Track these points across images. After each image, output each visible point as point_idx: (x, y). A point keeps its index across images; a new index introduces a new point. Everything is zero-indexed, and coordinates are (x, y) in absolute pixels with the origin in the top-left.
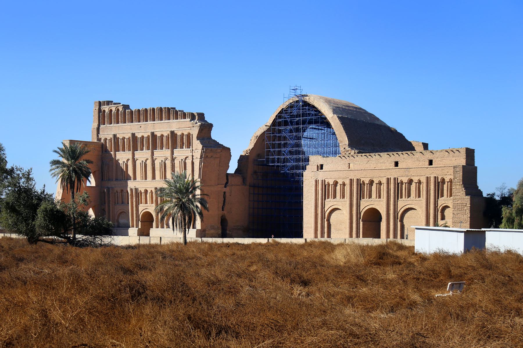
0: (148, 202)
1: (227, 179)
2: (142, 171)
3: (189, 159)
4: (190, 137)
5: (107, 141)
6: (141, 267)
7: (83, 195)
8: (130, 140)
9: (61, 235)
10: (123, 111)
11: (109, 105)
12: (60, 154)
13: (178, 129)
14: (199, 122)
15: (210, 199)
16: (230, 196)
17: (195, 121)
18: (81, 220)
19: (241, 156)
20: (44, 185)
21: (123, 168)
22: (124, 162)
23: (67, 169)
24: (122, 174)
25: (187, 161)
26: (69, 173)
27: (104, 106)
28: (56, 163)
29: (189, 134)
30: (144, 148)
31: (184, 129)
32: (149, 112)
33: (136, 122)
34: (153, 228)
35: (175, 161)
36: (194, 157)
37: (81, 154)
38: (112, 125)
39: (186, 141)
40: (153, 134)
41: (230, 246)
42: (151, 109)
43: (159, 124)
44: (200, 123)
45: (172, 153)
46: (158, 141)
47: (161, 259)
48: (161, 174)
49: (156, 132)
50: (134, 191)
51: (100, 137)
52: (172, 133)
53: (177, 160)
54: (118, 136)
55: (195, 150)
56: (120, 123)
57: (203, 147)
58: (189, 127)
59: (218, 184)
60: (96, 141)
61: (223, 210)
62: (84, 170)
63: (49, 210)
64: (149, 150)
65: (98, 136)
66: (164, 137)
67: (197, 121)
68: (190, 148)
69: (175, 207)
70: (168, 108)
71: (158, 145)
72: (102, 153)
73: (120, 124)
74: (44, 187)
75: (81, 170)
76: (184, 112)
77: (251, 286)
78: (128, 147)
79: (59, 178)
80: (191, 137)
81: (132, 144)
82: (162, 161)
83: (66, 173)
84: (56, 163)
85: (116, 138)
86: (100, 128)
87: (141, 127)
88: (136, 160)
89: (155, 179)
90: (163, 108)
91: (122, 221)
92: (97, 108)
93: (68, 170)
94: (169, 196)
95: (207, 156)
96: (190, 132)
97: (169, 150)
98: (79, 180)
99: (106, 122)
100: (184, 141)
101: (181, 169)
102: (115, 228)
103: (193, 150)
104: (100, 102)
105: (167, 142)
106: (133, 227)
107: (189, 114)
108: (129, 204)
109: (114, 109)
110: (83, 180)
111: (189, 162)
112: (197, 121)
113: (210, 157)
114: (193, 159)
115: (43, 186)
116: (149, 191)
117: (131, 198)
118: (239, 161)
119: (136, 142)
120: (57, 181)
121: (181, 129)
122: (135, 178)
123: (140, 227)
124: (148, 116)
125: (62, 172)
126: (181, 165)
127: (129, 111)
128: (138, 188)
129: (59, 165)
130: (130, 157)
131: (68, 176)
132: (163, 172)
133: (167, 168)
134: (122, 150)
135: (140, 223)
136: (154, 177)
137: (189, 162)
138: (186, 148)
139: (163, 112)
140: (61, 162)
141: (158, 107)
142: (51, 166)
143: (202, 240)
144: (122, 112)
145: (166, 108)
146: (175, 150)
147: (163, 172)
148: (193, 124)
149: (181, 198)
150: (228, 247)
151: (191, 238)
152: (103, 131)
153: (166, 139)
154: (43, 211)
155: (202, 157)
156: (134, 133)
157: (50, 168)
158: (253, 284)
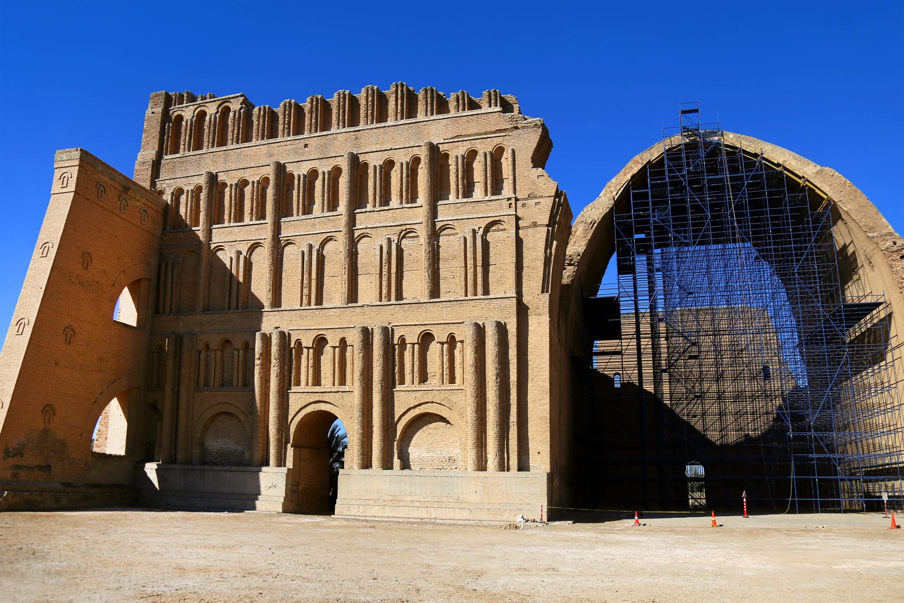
2: (306, 276)
21: (234, 272)
36: (520, 222)
55: (525, 199)
72: (163, 233)
78: (257, 207)
86: (163, 162)
88: (283, 243)
114: (518, 228)
117: (262, 365)
119: (285, 192)
128: (289, 334)
134: (235, 216)
135: (290, 451)
152: (173, 170)
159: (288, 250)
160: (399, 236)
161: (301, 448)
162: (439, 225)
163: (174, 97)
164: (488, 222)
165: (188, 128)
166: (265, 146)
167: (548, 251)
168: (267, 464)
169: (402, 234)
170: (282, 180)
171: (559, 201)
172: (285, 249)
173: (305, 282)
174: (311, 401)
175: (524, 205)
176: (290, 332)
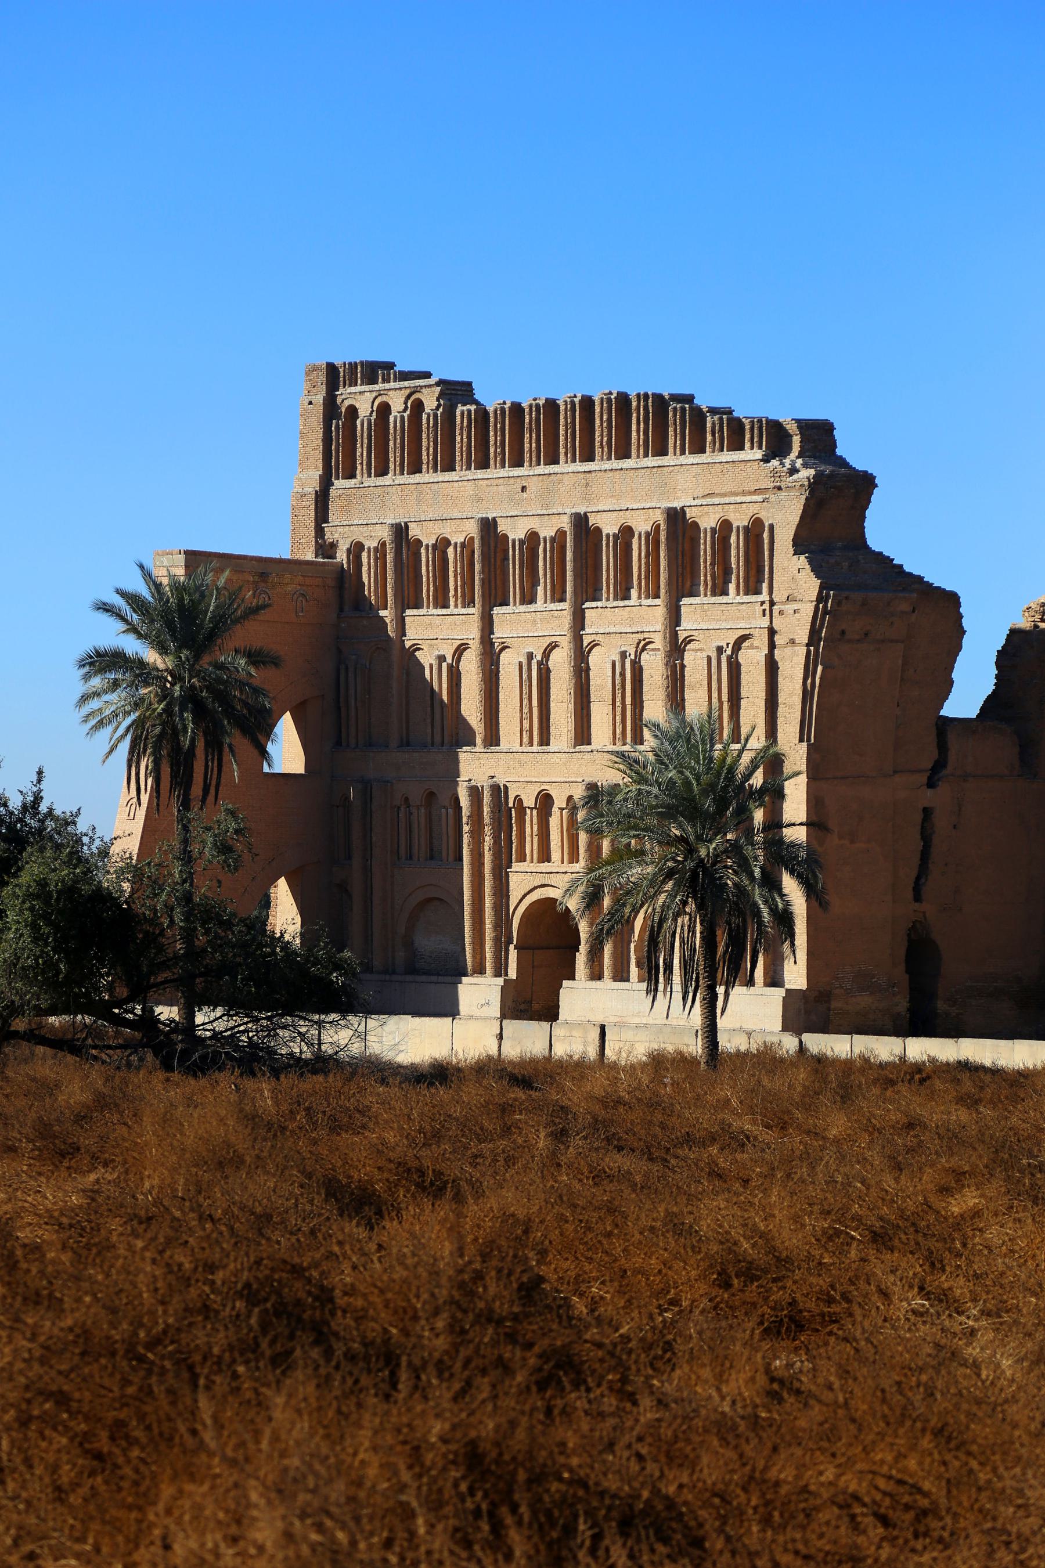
0: (555, 855)
1: (942, 746)
2: (525, 702)
3: (752, 647)
4: (759, 537)
5: (364, 555)
6: (423, 1181)
7: (218, 821)
8: (473, 552)
9: (116, 1011)
10: (441, 410)
11: (373, 381)
12: (124, 620)
13: (704, 502)
14: (805, 466)
15: (852, 842)
16: (955, 827)
17: (787, 462)
18: (208, 941)
19: (1014, 634)
20: (40, 773)
21: (436, 687)
22: (441, 659)
23: (157, 694)
24: (433, 719)
25: (743, 656)
26: (168, 711)
27: (353, 389)
28: (108, 666)
29: (757, 524)
30: (540, 590)
31: (732, 499)
32: (566, 418)
33: (503, 466)
34: (574, 979)
35: (688, 657)
36: (776, 638)
37: (223, 622)
38: (387, 480)
39: (742, 559)
40: (580, 521)
41: (929, 1077)
42: (577, 400)
43: (610, 474)
44: (812, 472)
45: (674, 617)
46: (604, 558)
47: (543, 1142)
48: (618, 718)
49: (599, 515)
50: (487, 799)
51: (329, 537)
52: (676, 517)
53: (697, 651)
54: (414, 532)
55: (782, 603)
56: (424, 470)
57: (821, 588)
58: (757, 491)
59: (895, 772)
60: (310, 556)
61: (917, 898)
62: (240, 700)
63: (57, 892)
64: (562, 600)
65: (320, 532)
66: (636, 536)
67: (800, 461)
68: (758, 592)
69: (664, 882)
70: (659, 398)
71: (604, 578)
72: (339, 616)
73: (426, 476)
74: (39, 781)
75: (222, 697)
76: (735, 414)
77: (928, 1293)
78: (463, 587)
79: (123, 737)
80: (766, 541)
81: (483, 572)
82: (623, 655)
83: (154, 710)
84: (108, 666)
85: (408, 540)
86: (332, 492)
87: (524, 489)
88: (497, 647)
89: (589, 743)
90: (633, 394)
91: (428, 943)
92: (319, 399)
93: (164, 697)
94: (636, 827)
95: (843, 632)
96: (763, 515)
97: (657, 601)
98: (215, 745)
99: (359, 467)
100: (733, 560)
101: (715, 695)
102: (395, 978)
103: (772, 603)
104: (332, 369)
105: (647, 564)
106: (480, 970)
107: (760, 428)
108: (461, 859)
109: (397, 403)
110: (230, 746)
111: (752, 660)
112: (799, 463)
113: (857, 637)
114: (772, 646)
115: (35, 778)
116: (560, 801)
117: (472, 832)
118: (1004, 659)
119: (498, 563)
120: (111, 751)
121: (716, 500)
122: (493, 738)
123: (512, 974)
124: (562, 438)
125: (136, 705)
126: (714, 677)
127: (469, 411)
128: (505, 787)
129: (119, 676)
130: (472, 633)
131: (163, 724)
132: (629, 708)
133: (645, 688)
134: (435, 598)
135: (513, 954)
136: (583, 735)
137: (752, 660)
138: (738, 594)
139: (634, 415)
140: (134, 661)
141: (611, 393)
142: (86, 678)
143: (801, 1042)
144: (435, 416)
145: (646, 396)
146: (685, 601)
147: (629, 708)
148: (774, 473)
149: (692, 838)
150: (922, 1081)
151: (749, 1034)
152: (346, 509)
153: (643, 547)
154: (29, 896)
155: (815, 638)
156: (494, 519)
157: (81, 688)
158: (944, 1281)
159: (505, 658)
160: (637, 647)
161: (534, 949)
162: (682, 636)
163: (341, 370)
164: (736, 637)
165: (365, 435)
166: (470, 483)
167: (809, 681)
168: (572, 977)
169: (641, 645)
170: (492, 548)
171: (825, 606)
172: (502, 655)
173: (526, 710)
174: (536, 885)
175: (781, 613)
176: (508, 784)
